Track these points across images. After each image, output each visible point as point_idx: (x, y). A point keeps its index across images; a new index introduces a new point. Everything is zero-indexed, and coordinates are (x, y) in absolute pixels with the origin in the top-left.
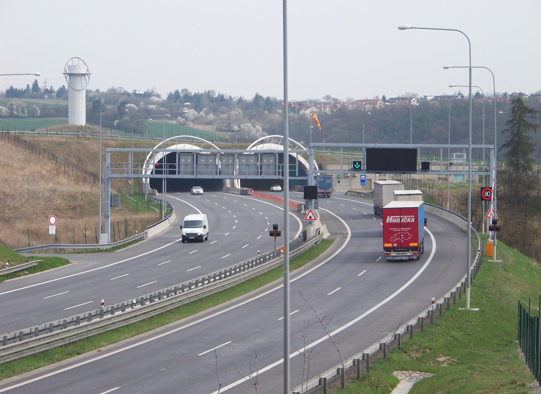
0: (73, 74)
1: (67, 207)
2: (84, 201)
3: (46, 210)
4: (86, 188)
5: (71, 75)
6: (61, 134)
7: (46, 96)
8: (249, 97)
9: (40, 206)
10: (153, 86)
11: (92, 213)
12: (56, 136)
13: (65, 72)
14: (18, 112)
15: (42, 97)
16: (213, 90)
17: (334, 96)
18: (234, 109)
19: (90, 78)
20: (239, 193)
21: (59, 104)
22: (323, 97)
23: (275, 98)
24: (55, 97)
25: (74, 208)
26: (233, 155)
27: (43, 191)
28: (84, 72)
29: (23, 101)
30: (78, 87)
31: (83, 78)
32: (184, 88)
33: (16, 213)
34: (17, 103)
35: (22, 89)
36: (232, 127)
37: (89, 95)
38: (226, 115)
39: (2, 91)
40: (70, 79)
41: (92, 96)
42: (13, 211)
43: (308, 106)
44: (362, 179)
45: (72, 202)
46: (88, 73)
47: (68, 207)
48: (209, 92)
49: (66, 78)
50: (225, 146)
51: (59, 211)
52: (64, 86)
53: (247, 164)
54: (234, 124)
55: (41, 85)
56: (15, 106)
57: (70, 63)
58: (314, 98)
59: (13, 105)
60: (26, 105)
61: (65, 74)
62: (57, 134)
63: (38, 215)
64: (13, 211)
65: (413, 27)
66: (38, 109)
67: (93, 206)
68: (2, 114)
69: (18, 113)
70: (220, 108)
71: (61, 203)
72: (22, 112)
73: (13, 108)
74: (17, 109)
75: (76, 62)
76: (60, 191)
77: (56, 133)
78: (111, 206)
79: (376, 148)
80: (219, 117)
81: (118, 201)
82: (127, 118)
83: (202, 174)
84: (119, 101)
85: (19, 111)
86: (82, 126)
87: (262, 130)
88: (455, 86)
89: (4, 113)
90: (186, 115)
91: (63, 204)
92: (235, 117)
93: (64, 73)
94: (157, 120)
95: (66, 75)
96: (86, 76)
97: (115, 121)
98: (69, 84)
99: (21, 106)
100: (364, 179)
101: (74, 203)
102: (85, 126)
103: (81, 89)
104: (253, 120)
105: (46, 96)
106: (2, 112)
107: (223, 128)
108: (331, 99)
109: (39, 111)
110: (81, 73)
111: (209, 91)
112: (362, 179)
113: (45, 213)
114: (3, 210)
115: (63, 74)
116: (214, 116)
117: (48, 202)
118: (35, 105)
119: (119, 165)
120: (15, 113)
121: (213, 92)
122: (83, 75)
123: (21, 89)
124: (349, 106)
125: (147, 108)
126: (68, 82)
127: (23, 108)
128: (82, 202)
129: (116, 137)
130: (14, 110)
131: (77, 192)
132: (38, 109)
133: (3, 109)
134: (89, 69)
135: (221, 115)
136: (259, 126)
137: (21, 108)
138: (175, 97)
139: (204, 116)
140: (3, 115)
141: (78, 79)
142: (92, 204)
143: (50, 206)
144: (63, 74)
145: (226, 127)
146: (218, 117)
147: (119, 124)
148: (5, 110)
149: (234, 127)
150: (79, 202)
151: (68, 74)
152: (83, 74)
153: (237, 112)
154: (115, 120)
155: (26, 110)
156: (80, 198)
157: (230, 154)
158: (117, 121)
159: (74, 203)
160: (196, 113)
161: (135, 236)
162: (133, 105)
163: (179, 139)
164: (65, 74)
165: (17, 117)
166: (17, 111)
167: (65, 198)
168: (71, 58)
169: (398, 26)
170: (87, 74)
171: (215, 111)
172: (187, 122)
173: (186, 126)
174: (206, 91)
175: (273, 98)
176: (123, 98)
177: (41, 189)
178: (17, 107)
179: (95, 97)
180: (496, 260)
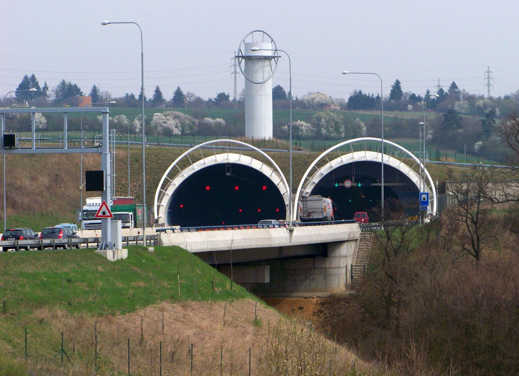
0: (250, 57)
5: (249, 59)
7: (410, 107)
13: (239, 54)
14: (328, 131)
15: (404, 108)
19: (277, 64)
28: (269, 54)
31: (267, 63)
34: (329, 115)
35: (373, 95)
37: (477, 103)
39: (343, 100)
41: (482, 105)
44: (422, 200)
46: (276, 55)
50: (298, 156)
55: (405, 89)
56: (323, 120)
57: (248, 40)
59: (321, 118)
60: (342, 120)
66: (362, 124)
72: (335, 129)
73: (321, 123)
88: (109, 23)
89: (305, 131)
95: (240, 59)
100: (426, 200)
103: (262, 81)
105: (410, 107)
106: (302, 130)
109: (365, 129)
112: (422, 200)
118: (358, 119)
119: (123, 188)
120: (324, 131)
123: (371, 95)
126: (243, 70)
127: (337, 124)
132: (362, 124)
133: (302, 125)
137: (334, 123)
140: (303, 135)
141: (259, 65)
147: (482, 148)
148: (307, 126)
151: (243, 57)
154: (476, 142)
155: (343, 127)
158: (480, 143)
163: (217, 145)
164: (238, 57)
166: (327, 128)
170: (274, 57)
178: (327, 122)
179: (485, 106)
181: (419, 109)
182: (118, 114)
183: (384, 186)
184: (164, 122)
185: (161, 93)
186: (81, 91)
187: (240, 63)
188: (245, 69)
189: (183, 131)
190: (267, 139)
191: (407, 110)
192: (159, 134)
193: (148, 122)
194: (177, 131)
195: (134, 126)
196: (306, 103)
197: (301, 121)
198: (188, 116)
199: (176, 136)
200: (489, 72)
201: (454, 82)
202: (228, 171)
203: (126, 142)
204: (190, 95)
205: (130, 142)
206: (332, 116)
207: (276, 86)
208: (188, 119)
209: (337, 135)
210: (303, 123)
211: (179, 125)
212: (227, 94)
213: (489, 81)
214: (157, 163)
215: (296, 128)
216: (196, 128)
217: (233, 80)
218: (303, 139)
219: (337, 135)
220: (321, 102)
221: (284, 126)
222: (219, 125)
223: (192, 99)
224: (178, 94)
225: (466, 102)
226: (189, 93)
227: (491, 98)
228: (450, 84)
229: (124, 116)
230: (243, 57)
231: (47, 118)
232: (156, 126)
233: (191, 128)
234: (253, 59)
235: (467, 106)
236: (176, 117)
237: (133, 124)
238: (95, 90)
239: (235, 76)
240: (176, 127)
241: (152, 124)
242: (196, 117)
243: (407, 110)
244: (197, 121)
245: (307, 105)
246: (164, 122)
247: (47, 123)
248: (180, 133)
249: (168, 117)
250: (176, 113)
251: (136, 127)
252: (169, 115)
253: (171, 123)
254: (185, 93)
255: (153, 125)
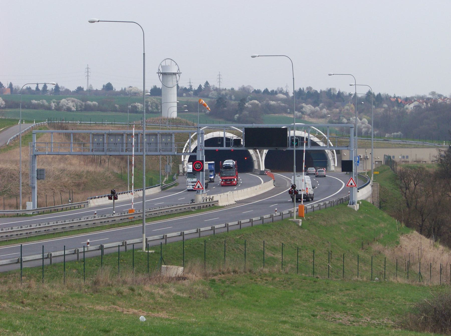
0: (165, 73)
1: (72, 184)
2: (88, 179)
3: (54, 186)
4: (91, 168)
5: (164, 74)
6: (115, 124)
7: (184, 94)
8: (362, 92)
9: (49, 183)
10: (286, 85)
11: (94, 189)
12: (111, 125)
13: (158, 71)
14: (152, 108)
16: (334, 88)
17: (438, 92)
18: (348, 104)
20: (259, 173)
21: (189, 101)
22: (429, 93)
23: (388, 94)
24: (192, 95)
25: (78, 185)
26: (156, 135)
27: (54, 171)
28: (175, 71)
29: (157, 98)
30: (170, 85)
31: (174, 76)
32: (308, 86)
33: (28, 189)
34: (152, 100)
36: (342, 120)
38: (338, 110)
40: (163, 77)
42: (26, 187)
43: (412, 101)
45: (77, 180)
46: (179, 72)
47: (73, 184)
48: (330, 89)
49: (159, 77)
51: (66, 187)
52: (200, 85)
53: (165, 142)
54: (343, 117)
55: (322, 90)
56: (149, 103)
57: (163, 64)
58: (421, 94)
61: (158, 73)
62: (112, 124)
63: (47, 191)
64: (26, 187)
65: (100, 20)
67: (96, 183)
68: (138, 109)
69: (152, 109)
70: (335, 103)
71: (68, 181)
72: (156, 107)
73: (148, 104)
74: (152, 105)
75: (168, 62)
76: (69, 170)
77: (111, 123)
78: (38, 179)
79: (253, 127)
80: (332, 112)
81: (43, 175)
82: (245, 112)
83: (112, 151)
84: (248, 98)
85: (153, 107)
86: (173, 119)
87: (368, 122)
88: (333, 74)
89: (140, 109)
90: (304, 110)
91: (69, 182)
92: (346, 111)
93: (158, 72)
94: (277, 115)
95: (160, 74)
96: (177, 75)
97: (236, 116)
98: (163, 82)
99: (155, 103)
101: (80, 180)
102: (176, 118)
103: (172, 86)
104: (361, 114)
105: (184, 94)
106: (138, 108)
107: (334, 121)
108: (436, 95)
110: (172, 72)
111: (330, 89)
113: (53, 189)
114: (17, 187)
115: (157, 73)
116: (328, 111)
117: (57, 179)
120: (150, 109)
121: (334, 89)
122: (175, 74)
124: (447, 101)
125: (269, 103)
126: (161, 81)
128: (86, 180)
129: (165, 126)
130: (149, 106)
131: (83, 171)
134: (180, 69)
135: (334, 110)
136: (365, 119)
138: (300, 94)
139: (319, 110)
140: (139, 111)
141: (170, 78)
142: (95, 181)
143: (58, 183)
144: (157, 73)
145: (336, 120)
146: (331, 112)
147: (239, 118)
148: (141, 106)
149: (343, 120)
150: (84, 179)
151: (161, 73)
152: (174, 73)
153: (349, 107)
154: (235, 115)
156: (85, 176)
157: (164, 134)
158: (238, 115)
159: (80, 180)
160: (313, 108)
161: (68, 204)
162: (256, 101)
164: (158, 73)
165: (152, 112)
166: (151, 107)
167: (72, 176)
168: (164, 59)
169: (88, 20)
170: (178, 73)
171: (329, 106)
172: (303, 116)
173: (302, 119)
174: (328, 89)
175: (386, 95)
176: (251, 95)
177: (53, 168)
178: (152, 104)
180: (296, 219)
181: (190, 95)
182: (42, 99)
183: (296, 150)
184: (67, 104)
185: (47, 87)
186: (3, 85)
187: (159, 77)
188: (162, 80)
189: (77, 108)
190: (175, 118)
191: (183, 96)
192: (64, 110)
193: (58, 103)
194: (74, 109)
195: (51, 106)
196: (127, 92)
197: (138, 103)
198: (79, 100)
199: (73, 111)
200: (220, 75)
201: (207, 81)
202: (220, 141)
203: (159, 125)
204: (62, 88)
205: (161, 125)
206: (154, 101)
207: (108, 83)
208: (79, 102)
209: (157, 110)
210: (139, 104)
211: (75, 105)
212: (82, 87)
213: (220, 80)
214: (179, 137)
215: (136, 107)
216: (83, 107)
217: (87, 80)
218: (139, 113)
219: (157, 110)
220: (135, 92)
221: (129, 106)
222: (95, 105)
223: (63, 90)
224: (57, 87)
225: (216, 92)
226: (61, 87)
227: (219, 88)
228: (205, 82)
229: (45, 100)
230: (161, 73)
231: (5, 102)
232: (62, 106)
233: (81, 107)
234: (167, 74)
235: (216, 94)
236: (73, 101)
237: (51, 105)
238: (11, 85)
239: (88, 78)
240: (73, 106)
241: (60, 104)
242: (83, 101)
243: (183, 96)
244: (84, 103)
245: (128, 93)
246: (67, 104)
247: (5, 104)
248: (75, 110)
249: (69, 101)
250: (73, 99)
251: (52, 107)
252: (69, 100)
253: (71, 104)
254: (60, 86)
255: (61, 105)
